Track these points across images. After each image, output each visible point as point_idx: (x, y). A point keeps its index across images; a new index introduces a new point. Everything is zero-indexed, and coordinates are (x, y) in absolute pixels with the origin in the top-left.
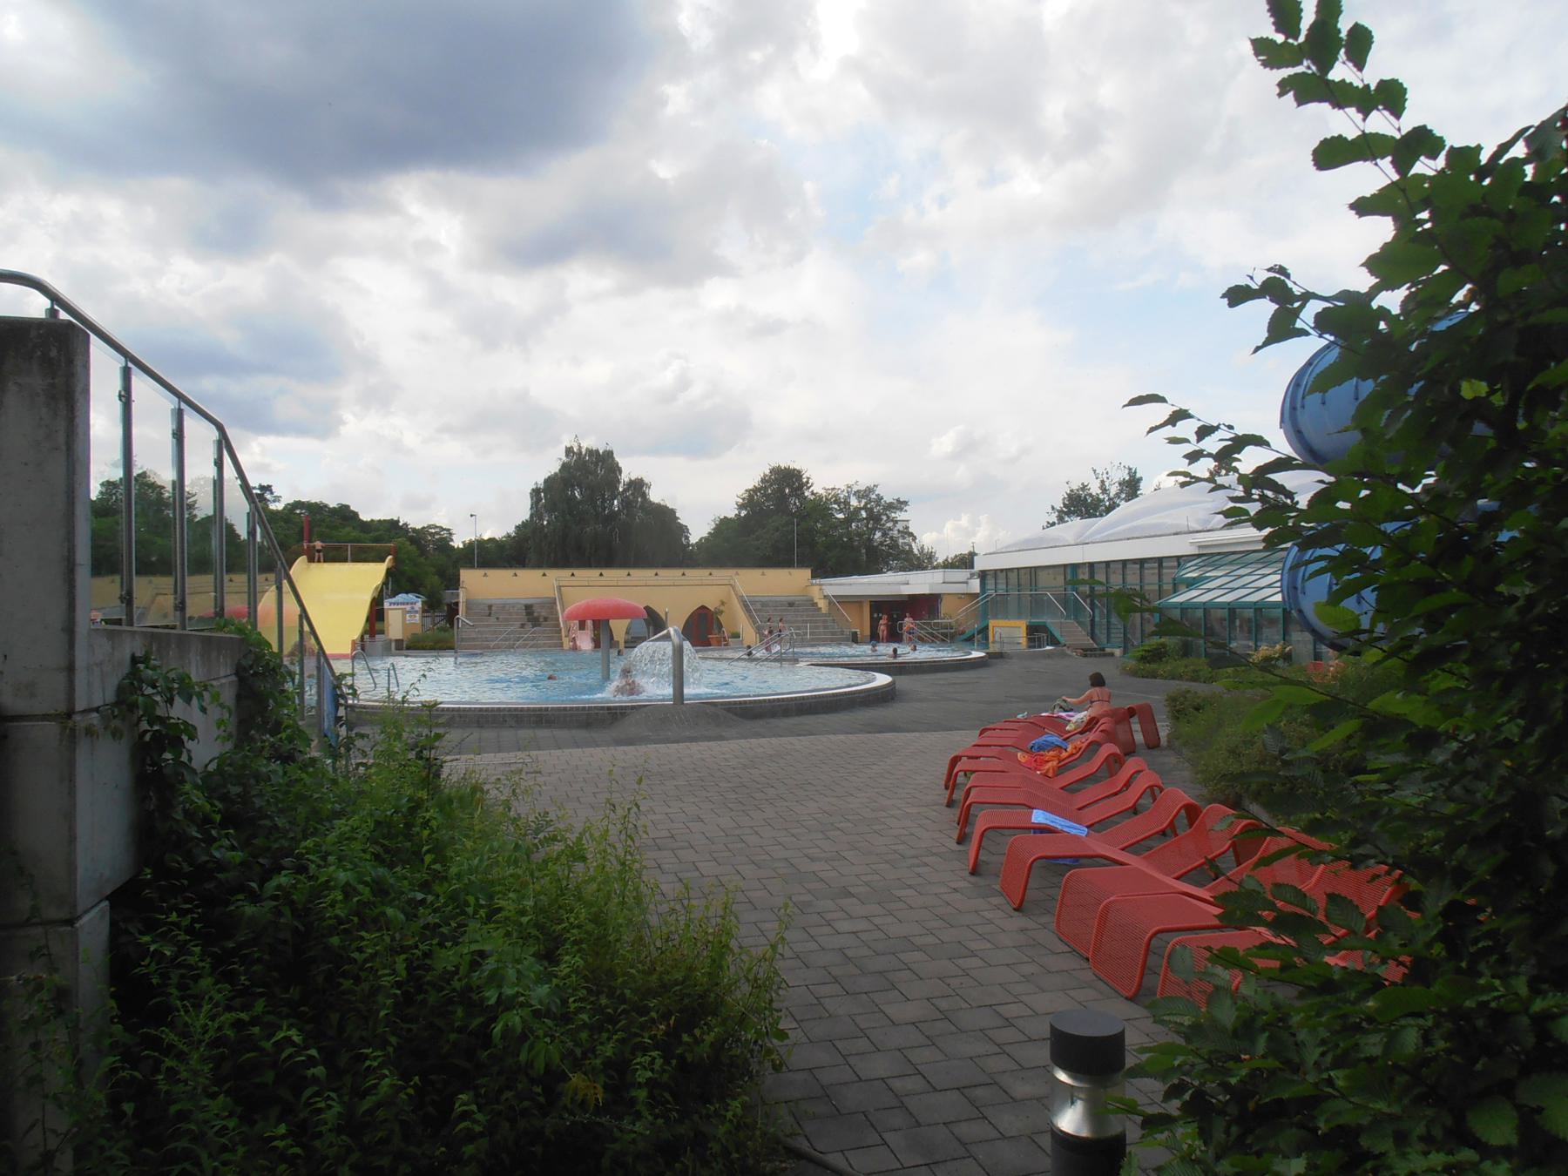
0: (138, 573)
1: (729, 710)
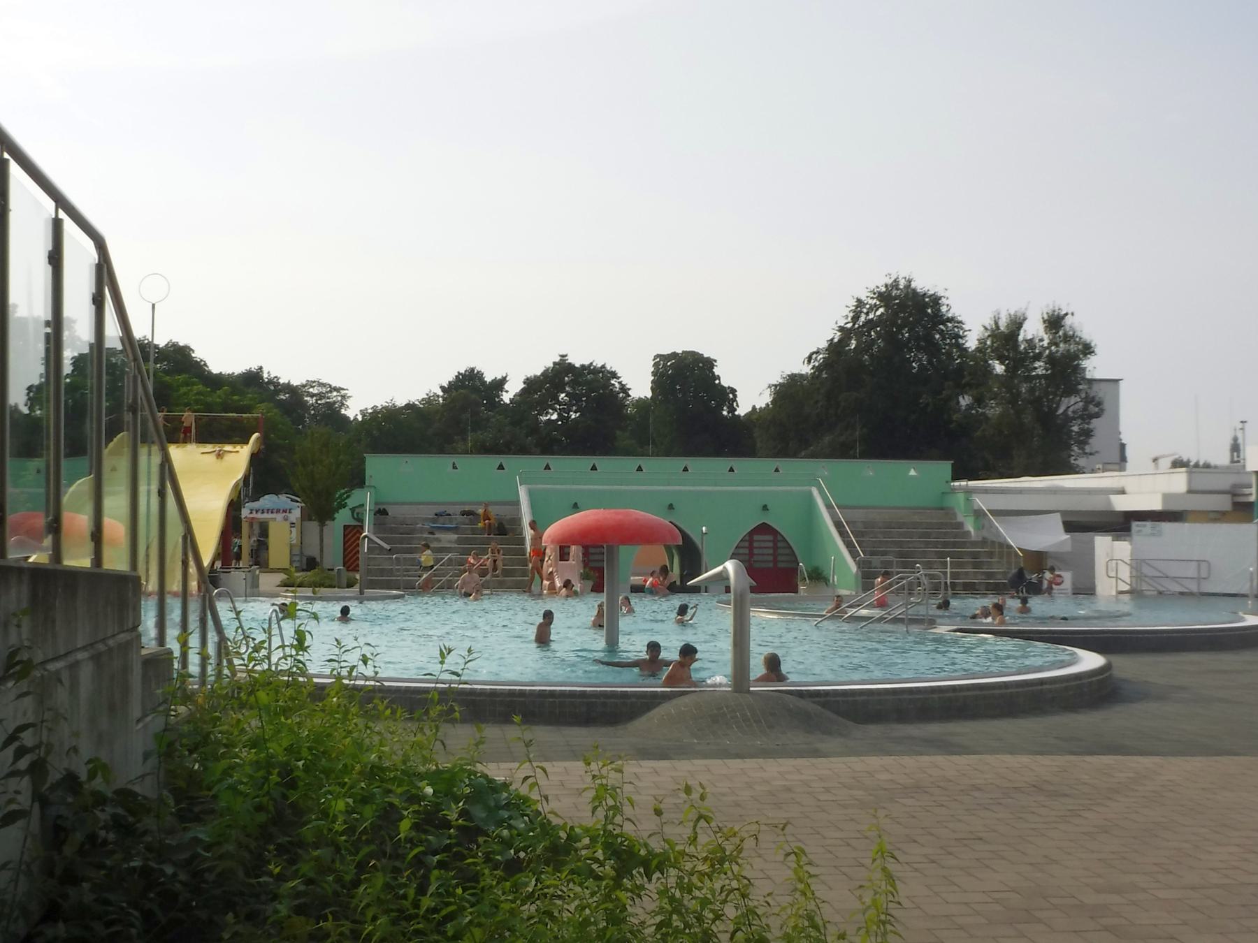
0: (67, 456)
1: (824, 705)
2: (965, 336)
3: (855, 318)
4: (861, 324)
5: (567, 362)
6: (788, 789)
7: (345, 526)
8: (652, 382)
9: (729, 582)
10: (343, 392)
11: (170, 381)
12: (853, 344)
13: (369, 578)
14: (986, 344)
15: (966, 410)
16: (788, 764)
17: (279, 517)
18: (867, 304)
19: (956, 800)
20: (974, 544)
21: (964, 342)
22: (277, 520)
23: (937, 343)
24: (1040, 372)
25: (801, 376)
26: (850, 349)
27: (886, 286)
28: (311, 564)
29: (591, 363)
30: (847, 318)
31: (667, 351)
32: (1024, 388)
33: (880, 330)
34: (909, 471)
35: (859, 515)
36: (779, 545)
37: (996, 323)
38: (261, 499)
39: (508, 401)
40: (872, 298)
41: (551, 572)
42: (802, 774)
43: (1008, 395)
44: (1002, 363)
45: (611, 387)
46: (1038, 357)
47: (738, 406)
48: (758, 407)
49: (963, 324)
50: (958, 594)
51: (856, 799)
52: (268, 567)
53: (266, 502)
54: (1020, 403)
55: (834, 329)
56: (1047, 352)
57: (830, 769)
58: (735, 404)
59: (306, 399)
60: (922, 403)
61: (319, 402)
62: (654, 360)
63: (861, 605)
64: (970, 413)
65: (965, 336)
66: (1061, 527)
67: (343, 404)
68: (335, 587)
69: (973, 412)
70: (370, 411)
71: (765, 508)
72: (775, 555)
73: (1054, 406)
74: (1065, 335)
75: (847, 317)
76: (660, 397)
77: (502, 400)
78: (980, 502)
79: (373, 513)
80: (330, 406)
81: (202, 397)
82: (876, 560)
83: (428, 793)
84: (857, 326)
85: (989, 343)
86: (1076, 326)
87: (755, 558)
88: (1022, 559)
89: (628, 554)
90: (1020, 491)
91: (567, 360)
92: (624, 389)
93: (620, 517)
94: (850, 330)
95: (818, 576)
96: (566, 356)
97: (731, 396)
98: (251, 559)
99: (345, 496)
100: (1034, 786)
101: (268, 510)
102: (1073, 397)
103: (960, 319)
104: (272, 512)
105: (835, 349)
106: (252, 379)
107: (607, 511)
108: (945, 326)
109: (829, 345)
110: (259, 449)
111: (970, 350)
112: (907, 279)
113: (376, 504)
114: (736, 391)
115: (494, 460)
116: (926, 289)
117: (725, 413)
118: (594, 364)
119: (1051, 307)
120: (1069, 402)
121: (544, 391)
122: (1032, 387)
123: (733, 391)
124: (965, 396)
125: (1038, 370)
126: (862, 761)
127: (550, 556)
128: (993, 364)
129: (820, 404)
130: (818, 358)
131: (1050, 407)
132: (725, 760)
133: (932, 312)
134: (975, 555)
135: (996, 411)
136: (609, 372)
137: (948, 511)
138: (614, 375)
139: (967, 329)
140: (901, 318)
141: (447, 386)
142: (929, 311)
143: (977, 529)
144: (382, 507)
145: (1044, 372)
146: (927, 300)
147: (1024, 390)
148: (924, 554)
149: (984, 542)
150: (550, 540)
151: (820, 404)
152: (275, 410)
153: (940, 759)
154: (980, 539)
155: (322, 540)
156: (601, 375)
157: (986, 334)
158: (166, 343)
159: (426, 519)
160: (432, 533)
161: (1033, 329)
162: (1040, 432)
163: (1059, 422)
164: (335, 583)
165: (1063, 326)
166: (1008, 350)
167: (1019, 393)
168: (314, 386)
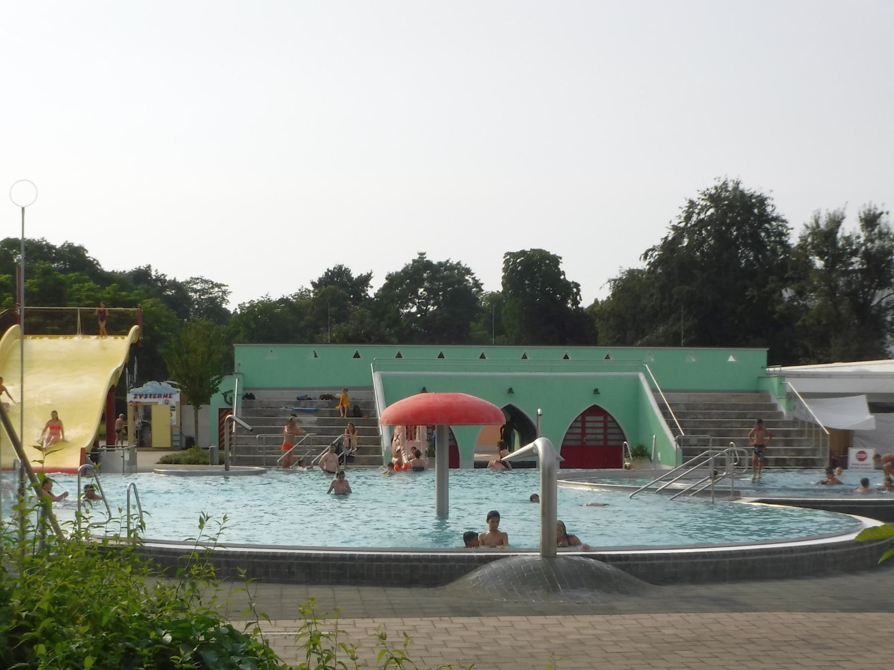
1: (623, 568)
2: (788, 234)
3: (688, 218)
4: (693, 223)
5: (425, 260)
6: (581, 643)
7: (219, 409)
8: (503, 277)
9: (539, 459)
10: (223, 288)
11: (63, 278)
12: (686, 242)
13: (237, 456)
14: (806, 241)
15: (788, 301)
16: (584, 620)
17: (161, 401)
18: (698, 205)
19: (730, 652)
20: (787, 424)
21: (787, 239)
22: (159, 404)
23: (763, 240)
24: (856, 266)
25: (640, 271)
26: (683, 247)
27: (716, 188)
28: (190, 442)
29: (448, 261)
30: (680, 218)
31: (516, 249)
32: (841, 282)
33: (710, 229)
34: (728, 357)
35: (680, 398)
36: (609, 425)
37: (817, 222)
38: (144, 385)
39: (372, 296)
40: (703, 199)
41: (399, 451)
42: (596, 629)
43: (826, 288)
44: (822, 258)
45: (465, 283)
46: (854, 253)
47: (581, 299)
48: (600, 300)
49: (787, 223)
50: (769, 469)
51: (640, 652)
52: (151, 447)
53: (149, 387)
54: (837, 295)
55: (667, 228)
56: (863, 248)
57: (622, 625)
58: (578, 298)
59: (190, 294)
60: (748, 296)
61: (202, 297)
62: (504, 257)
63: (672, 480)
64: (793, 305)
65: (788, 234)
66: (866, 408)
67: (224, 299)
68: (208, 464)
69: (796, 303)
70: (247, 305)
71: (596, 391)
72: (605, 435)
73: (869, 298)
74: (880, 233)
75: (680, 217)
76: (510, 291)
77: (367, 295)
78: (792, 386)
79: (241, 397)
80: (212, 300)
81: (93, 293)
82: (694, 439)
83: (167, 640)
84: (689, 225)
85: (809, 240)
86: (891, 223)
87: (588, 437)
88: (828, 438)
89: (463, 433)
90: (830, 376)
91: (425, 258)
92: (477, 285)
93: (449, 400)
94: (683, 229)
95: (642, 453)
96: (424, 254)
97: (575, 290)
98: (136, 439)
99: (217, 382)
100: (803, 640)
101: (151, 395)
102: (886, 289)
103: (784, 218)
104: (154, 397)
105: (669, 246)
106: (142, 276)
107: (438, 394)
108: (770, 224)
109: (664, 242)
110: (139, 340)
111: (793, 247)
112: (735, 182)
113: (244, 389)
114: (579, 285)
115: (351, 349)
116: (752, 191)
117: (569, 305)
118: (450, 261)
119: (867, 207)
120: (882, 295)
121: (404, 286)
122: (849, 281)
123: (577, 286)
124: (788, 289)
125: (855, 265)
126: (652, 618)
127: (398, 436)
128: (813, 260)
129: (655, 297)
130: (654, 255)
131: (865, 299)
132: (528, 617)
133: (759, 212)
134: (787, 434)
135: (816, 303)
136: (464, 269)
137: (763, 394)
138: (468, 271)
139: (790, 227)
140: (730, 218)
141: (317, 282)
142: (756, 211)
143: (789, 410)
144: (249, 392)
145: (860, 266)
146: (754, 200)
147: (841, 283)
148: (740, 433)
149: (795, 422)
150: (386, 420)
151: (655, 297)
152: (162, 305)
153: (722, 616)
154: (791, 419)
155: (196, 422)
156: (456, 271)
157: (808, 232)
158: (62, 244)
159: (290, 403)
160: (295, 415)
161: (851, 227)
162: (856, 321)
163: (873, 312)
164: (209, 460)
165: (878, 224)
166: (827, 247)
167: (836, 287)
168: (198, 283)
